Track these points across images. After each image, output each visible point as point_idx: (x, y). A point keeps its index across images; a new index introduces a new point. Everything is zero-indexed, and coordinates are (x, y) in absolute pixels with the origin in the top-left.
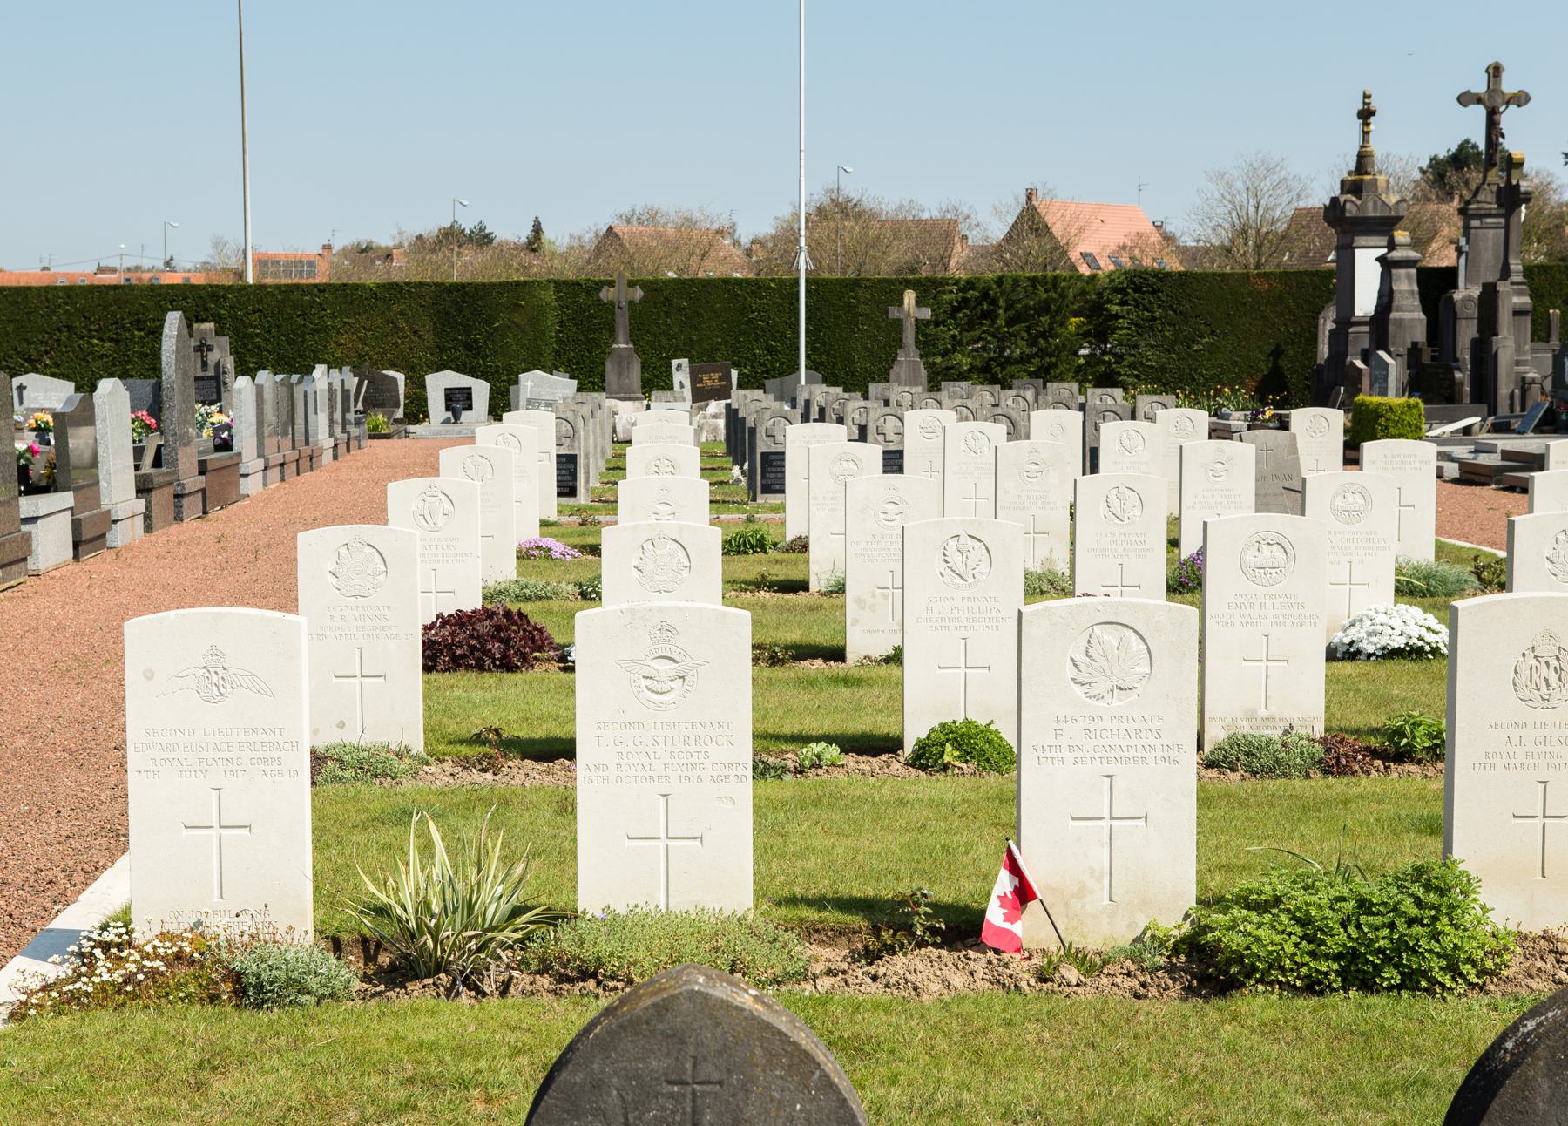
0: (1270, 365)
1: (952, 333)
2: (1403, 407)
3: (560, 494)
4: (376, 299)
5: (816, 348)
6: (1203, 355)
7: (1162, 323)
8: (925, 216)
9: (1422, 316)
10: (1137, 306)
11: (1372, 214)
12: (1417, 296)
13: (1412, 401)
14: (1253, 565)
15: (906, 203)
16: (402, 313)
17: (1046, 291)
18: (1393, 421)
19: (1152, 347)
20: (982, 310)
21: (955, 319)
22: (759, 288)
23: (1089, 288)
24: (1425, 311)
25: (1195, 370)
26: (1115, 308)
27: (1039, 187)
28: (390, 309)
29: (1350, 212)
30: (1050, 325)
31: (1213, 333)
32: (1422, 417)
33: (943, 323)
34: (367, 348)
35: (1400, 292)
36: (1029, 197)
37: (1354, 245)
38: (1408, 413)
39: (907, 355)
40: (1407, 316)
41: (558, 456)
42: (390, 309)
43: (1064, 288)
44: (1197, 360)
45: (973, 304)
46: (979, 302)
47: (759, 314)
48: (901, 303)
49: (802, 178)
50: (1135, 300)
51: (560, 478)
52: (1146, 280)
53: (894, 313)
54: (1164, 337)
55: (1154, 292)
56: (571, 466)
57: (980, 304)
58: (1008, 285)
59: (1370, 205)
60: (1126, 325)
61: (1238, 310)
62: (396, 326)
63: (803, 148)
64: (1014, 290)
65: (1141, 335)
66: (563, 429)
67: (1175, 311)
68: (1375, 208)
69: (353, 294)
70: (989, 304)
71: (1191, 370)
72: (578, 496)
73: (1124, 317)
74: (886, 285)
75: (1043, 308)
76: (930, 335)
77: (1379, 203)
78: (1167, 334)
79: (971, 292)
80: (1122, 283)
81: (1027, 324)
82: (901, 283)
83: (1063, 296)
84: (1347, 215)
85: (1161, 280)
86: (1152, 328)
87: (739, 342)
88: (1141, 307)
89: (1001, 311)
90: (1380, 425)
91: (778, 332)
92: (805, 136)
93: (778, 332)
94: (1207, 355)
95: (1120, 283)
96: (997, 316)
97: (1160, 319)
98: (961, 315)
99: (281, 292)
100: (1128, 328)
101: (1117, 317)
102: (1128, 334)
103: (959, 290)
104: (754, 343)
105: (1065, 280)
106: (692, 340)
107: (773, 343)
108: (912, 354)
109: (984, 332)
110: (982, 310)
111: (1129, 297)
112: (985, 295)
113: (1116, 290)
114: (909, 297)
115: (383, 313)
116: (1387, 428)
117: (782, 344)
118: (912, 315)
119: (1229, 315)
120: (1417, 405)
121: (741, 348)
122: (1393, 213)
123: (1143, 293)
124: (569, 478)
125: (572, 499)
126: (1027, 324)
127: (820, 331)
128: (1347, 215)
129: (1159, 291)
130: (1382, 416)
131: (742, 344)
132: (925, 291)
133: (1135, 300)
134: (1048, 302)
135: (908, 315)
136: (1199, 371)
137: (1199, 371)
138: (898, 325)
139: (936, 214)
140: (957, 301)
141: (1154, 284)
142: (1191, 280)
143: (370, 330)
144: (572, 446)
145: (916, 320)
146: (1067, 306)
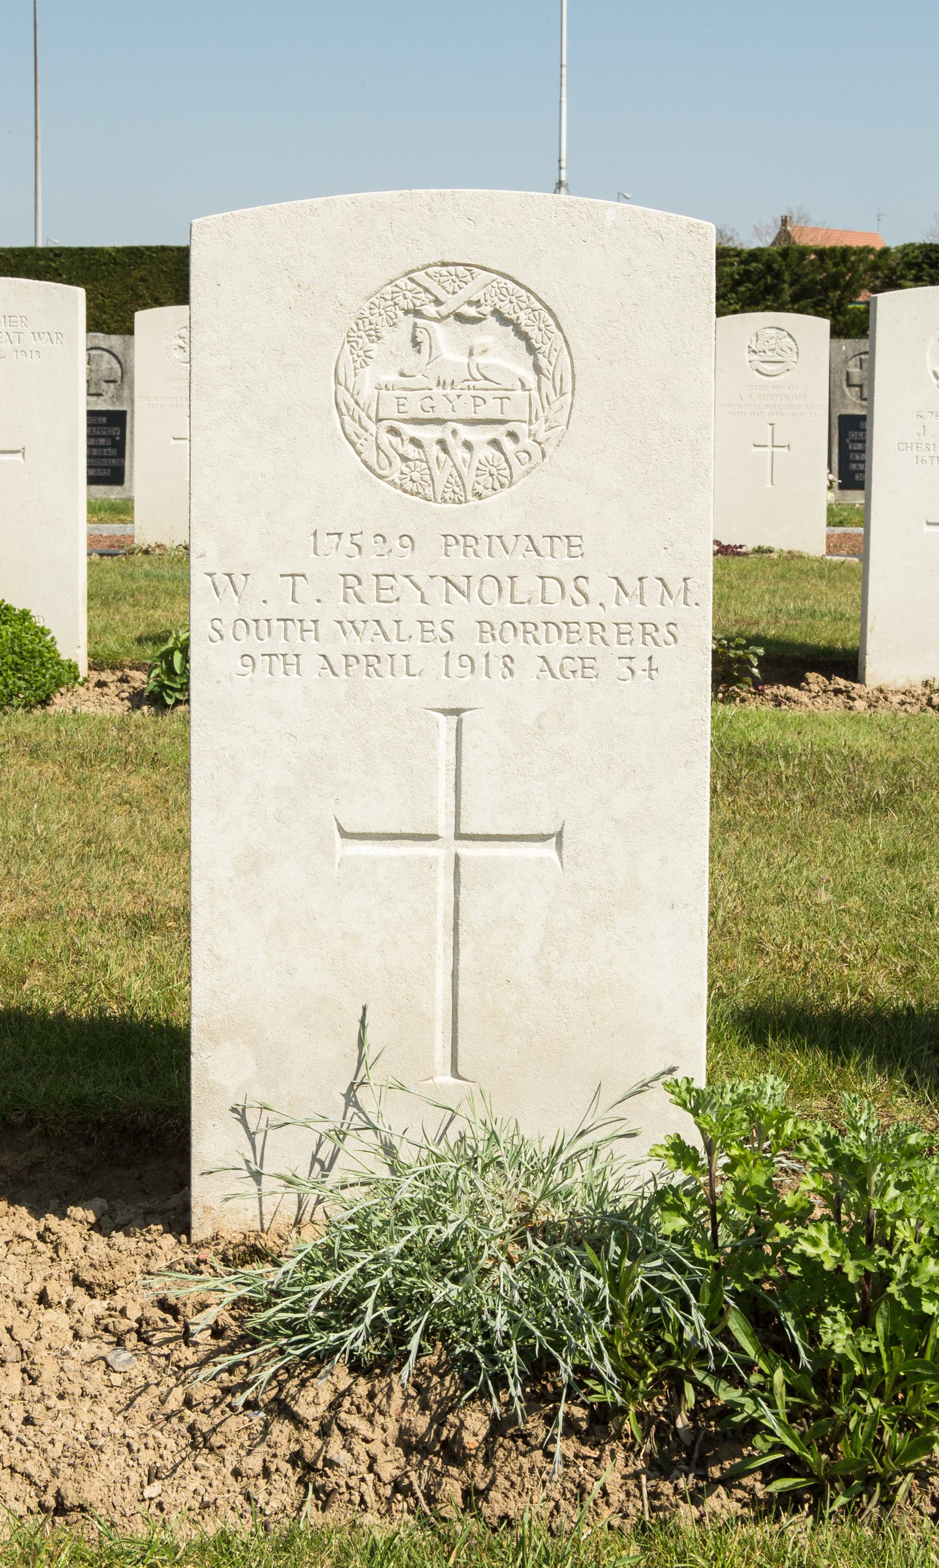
3: (92, 480)
4: (115, 264)
14: (389, 410)
16: (142, 279)
20: (766, 284)
21: (736, 292)
23: (881, 263)
27: (795, 219)
28: (129, 275)
34: (104, 316)
41: (90, 414)
42: (129, 275)
43: (853, 263)
45: (755, 278)
46: (762, 275)
49: (564, 99)
51: (95, 452)
56: (116, 431)
57: (764, 277)
62: (136, 294)
63: (564, 62)
64: (798, 265)
66: (104, 366)
69: (90, 259)
70: (773, 277)
72: (127, 484)
75: (834, 282)
79: (754, 264)
89: (786, 286)
92: (568, 48)
95: (914, 258)
96: (782, 290)
98: (742, 289)
99: (15, 256)
103: (740, 263)
105: (855, 253)
110: (766, 284)
112: (769, 268)
113: (909, 265)
115: (122, 279)
124: (112, 452)
125: (116, 489)
140: (738, 273)
143: (109, 297)
144: (118, 397)
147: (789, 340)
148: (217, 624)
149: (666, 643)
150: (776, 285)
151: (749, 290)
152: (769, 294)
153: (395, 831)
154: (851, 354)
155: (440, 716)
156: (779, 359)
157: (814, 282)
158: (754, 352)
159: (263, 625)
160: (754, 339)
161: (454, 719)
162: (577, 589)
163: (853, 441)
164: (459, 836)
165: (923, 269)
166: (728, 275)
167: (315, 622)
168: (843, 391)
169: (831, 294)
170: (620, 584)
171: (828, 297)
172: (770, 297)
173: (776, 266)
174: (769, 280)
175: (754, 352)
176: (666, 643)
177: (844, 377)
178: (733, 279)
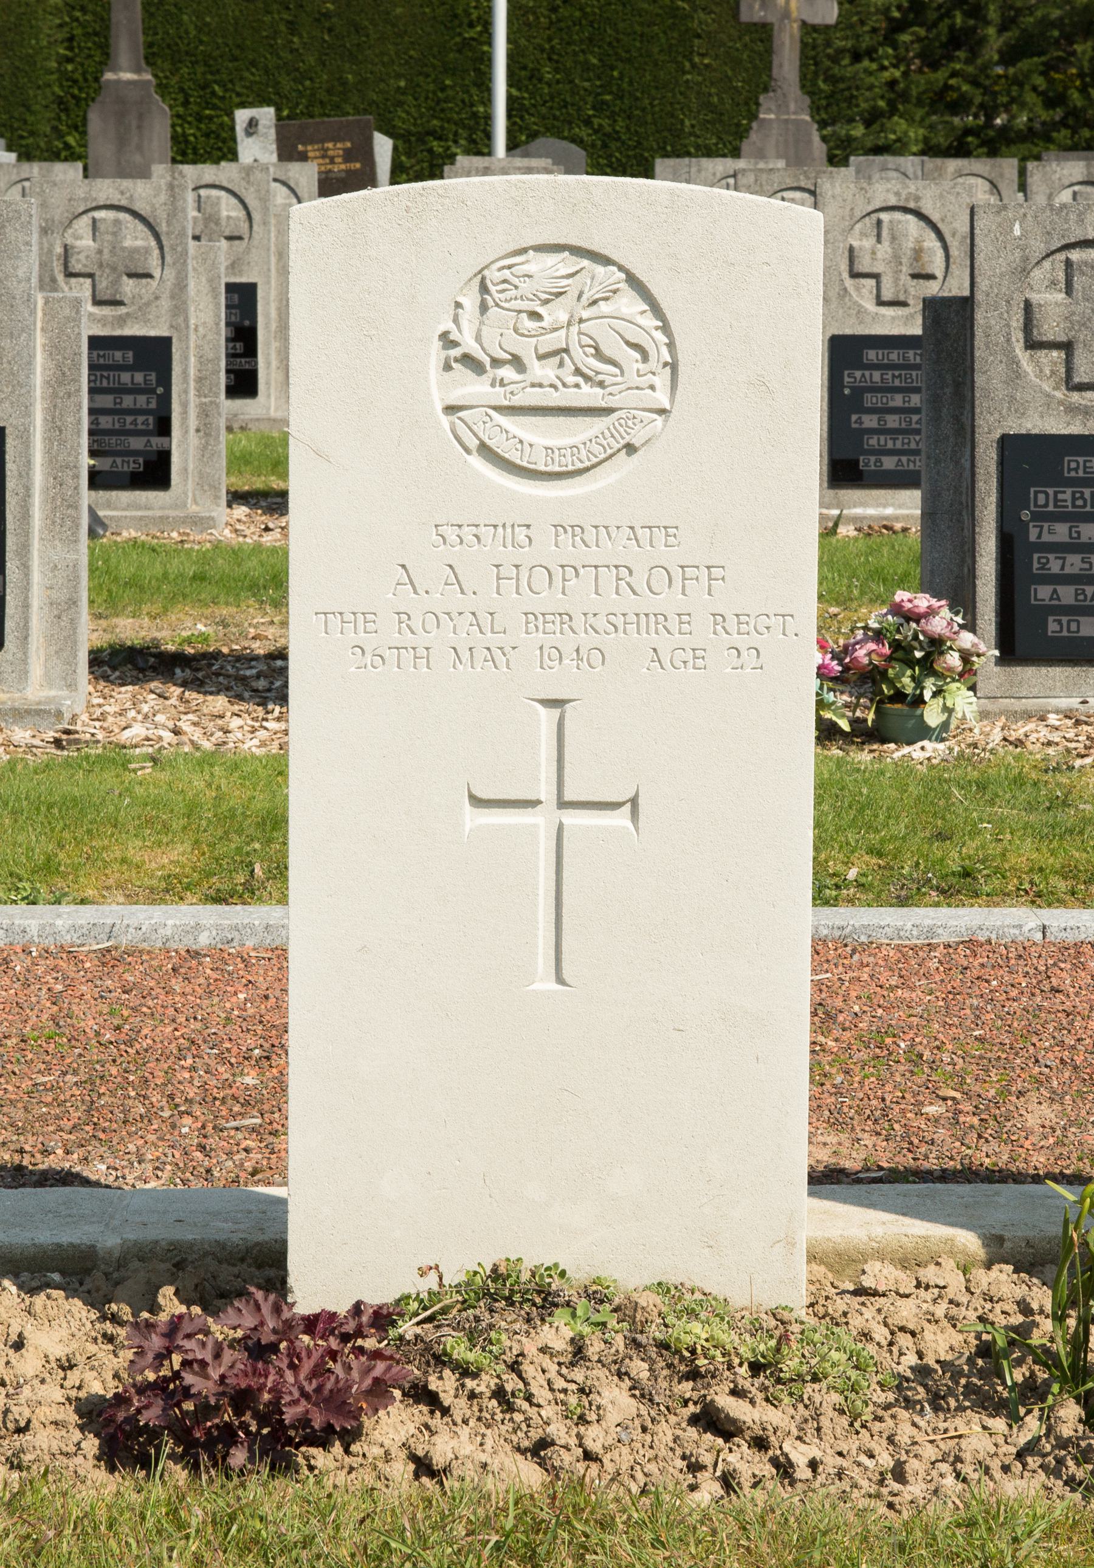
5: (603, 102)
20: (952, 28)
33: (870, 53)
39: (782, 107)
45: (932, 16)
76: (842, 79)
87: (443, 89)
89: (991, 31)
91: (525, 68)
96: (983, 41)
98: (905, 38)
108: (792, 106)
110: (952, 28)
117: (532, 95)
118: (794, 15)
121: (447, 100)
127: (612, 68)
131: (450, 93)
145: (804, 24)
147: (629, 304)
150: (974, 29)
151: (919, 40)
152: (958, 47)
153: (583, 798)
154: (1038, 247)
156: (589, 396)
157: (1046, 23)
158: (467, 360)
160: (470, 301)
163: (1040, 517)
166: (878, 11)
168: (1014, 362)
169: (1078, 48)
171: (1073, 53)
172: (961, 54)
174: (959, 20)
175: (467, 360)
177: (1017, 320)
178: (891, 20)
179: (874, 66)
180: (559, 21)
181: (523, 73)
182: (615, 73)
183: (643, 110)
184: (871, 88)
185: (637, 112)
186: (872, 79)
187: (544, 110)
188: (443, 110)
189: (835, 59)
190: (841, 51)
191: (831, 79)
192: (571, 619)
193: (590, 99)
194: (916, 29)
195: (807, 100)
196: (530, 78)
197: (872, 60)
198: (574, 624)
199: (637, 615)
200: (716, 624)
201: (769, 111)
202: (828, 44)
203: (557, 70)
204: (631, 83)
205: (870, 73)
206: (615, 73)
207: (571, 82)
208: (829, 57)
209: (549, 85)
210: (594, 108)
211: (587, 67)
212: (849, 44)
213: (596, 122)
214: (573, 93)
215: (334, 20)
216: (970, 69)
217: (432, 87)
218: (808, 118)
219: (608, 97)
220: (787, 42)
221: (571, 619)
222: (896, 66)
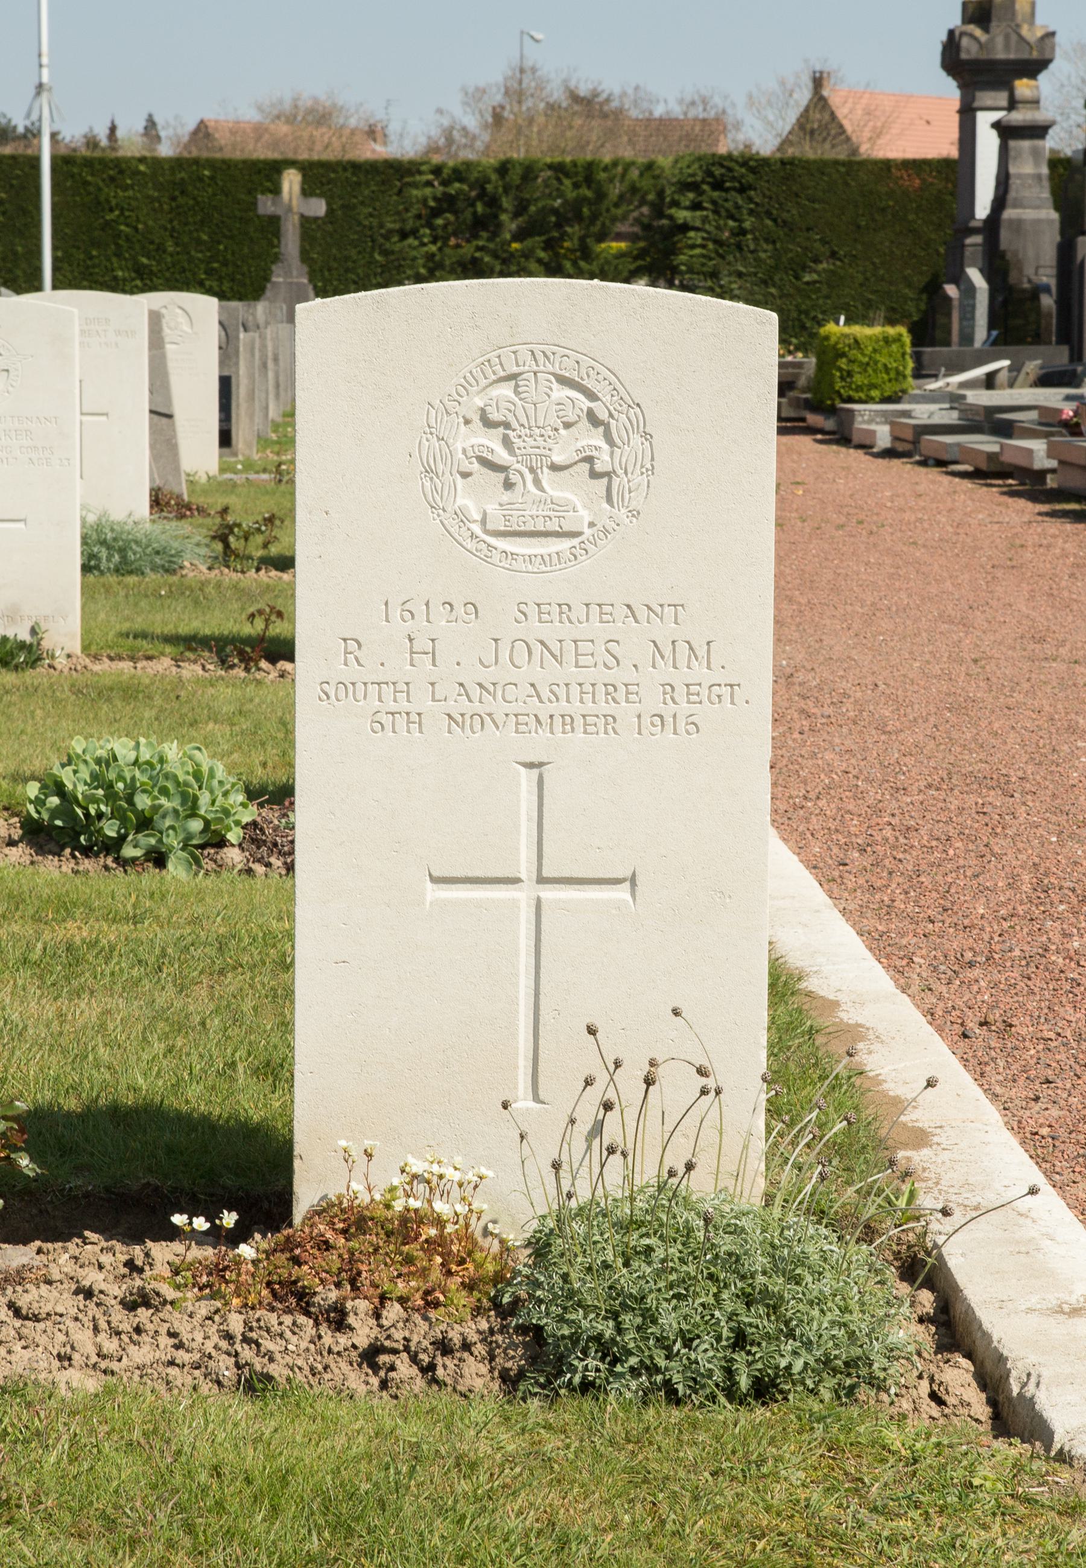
0: (923, 307)
1: (425, 249)
2: (877, 341)
5: (213, 269)
6: (819, 290)
7: (755, 239)
8: (659, 111)
9: (1055, 215)
10: (716, 212)
11: (1001, 55)
12: (1046, 184)
13: (891, 331)
15: (630, 91)
17: (576, 186)
18: (861, 364)
19: (740, 275)
20: (475, 213)
22: (121, 172)
24: (1057, 208)
25: (806, 313)
26: (682, 215)
29: (968, 51)
30: (582, 239)
31: (834, 254)
32: (908, 357)
33: (414, 233)
35: (1019, 176)
36: (818, 82)
37: (976, 104)
38: (885, 351)
39: (288, 274)
40: (1028, 214)
44: (809, 297)
47: (122, 213)
48: (276, 191)
50: (714, 202)
52: (730, 170)
53: (266, 205)
54: (758, 260)
55: (742, 190)
58: (515, 177)
59: (1000, 41)
60: (699, 241)
61: (874, 220)
65: (722, 257)
67: (775, 220)
68: (1007, 47)
70: (486, 204)
71: (800, 312)
73: (697, 229)
74: (321, 171)
75: (573, 212)
76: (393, 252)
77: (1014, 38)
78: (763, 255)
79: (457, 185)
80: (693, 175)
81: (543, 238)
82: (345, 169)
83: (601, 196)
84: (964, 56)
85: (753, 170)
86: (739, 247)
87: (91, 258)
88: (723, 213)
90: (840, 369)
91: (152, 242)
93: (152, 242)
94: (825, 290)
96: (499, 226)
97: (752, 231)
98: (439, 222)
100: (703, 246)
101: (685, 228)
102: (703, 256)
104: (114, 260)
106: (15, 253)
107: (144, 260)
108: (295, 273)
109: (479, 249)
111: (704, 198)
114: (291, 182)
116: (850, 374)
117: (159, 263)
118: (295, 210)
119: (859, 227)
120: (898, 339)
121: (94, 266)
122: (1035, 55)
123: (727, 190)
126: (543, 238)
127: (219, 243)
128: (964, 56)
129: (751, 187)
130: (843, 355)
131: (96, 261)
132: (383, 183)
133: (714, 202)
134: (581, 201)
135: (289, 209)
136: (813, 314)
137: (813, 314)
138: (273, 224)
139: (677, 111)
140: (435, 199)
141: (742, 176)
142: (800, 171)
145: (302, 216)
146: (608, 210)
148: (554, 687)
149: (550, 701)
153: (500, 875)
155: (522, 769)
159: (360, 687)
161: (535, 772)
162: (608, 651)
164: (541, 880)
165: (703, 192)
167: (407, 684)
170: (691, 648)
173: (489, 187)
176: (550, 701)
179: (416, 243)
180: (178, 207)
181: (151, 247)
182: (221, 247)
183: (243, 275)
184: (414, 259)
185: (239, 277)
186: (414, 253)
187: (168, 275)
188: (91, 274)
189: (387, 237)
190: (391, 231)
191: (385, 253)
192: (673, 688)
193: (202, 266)
194: (448, 215)
195: (306, 269)
196: (157, 250)
197: (416, 238)
198: (675, 695)
199: (593, 685)
200: (665, 693)
201: (279, 276)
202: (381, 226)
203: (177, 244)
204: (233, 254)
205: (414, 248)
206: (221, 247)
207: (188, 253)
208: (382, 235)
209: (172, 255)
210: (206, 273)
211: (199, 242)
212: (397, 226)
213: (208, 283)
214: (189, 262)
215: (7, 206)
216: (491, 246)
217: (82, 256)
218: (305, 281)
219: (216, 265)
220: (290, 227)
221: (673, 688)
222: (434, 242)
